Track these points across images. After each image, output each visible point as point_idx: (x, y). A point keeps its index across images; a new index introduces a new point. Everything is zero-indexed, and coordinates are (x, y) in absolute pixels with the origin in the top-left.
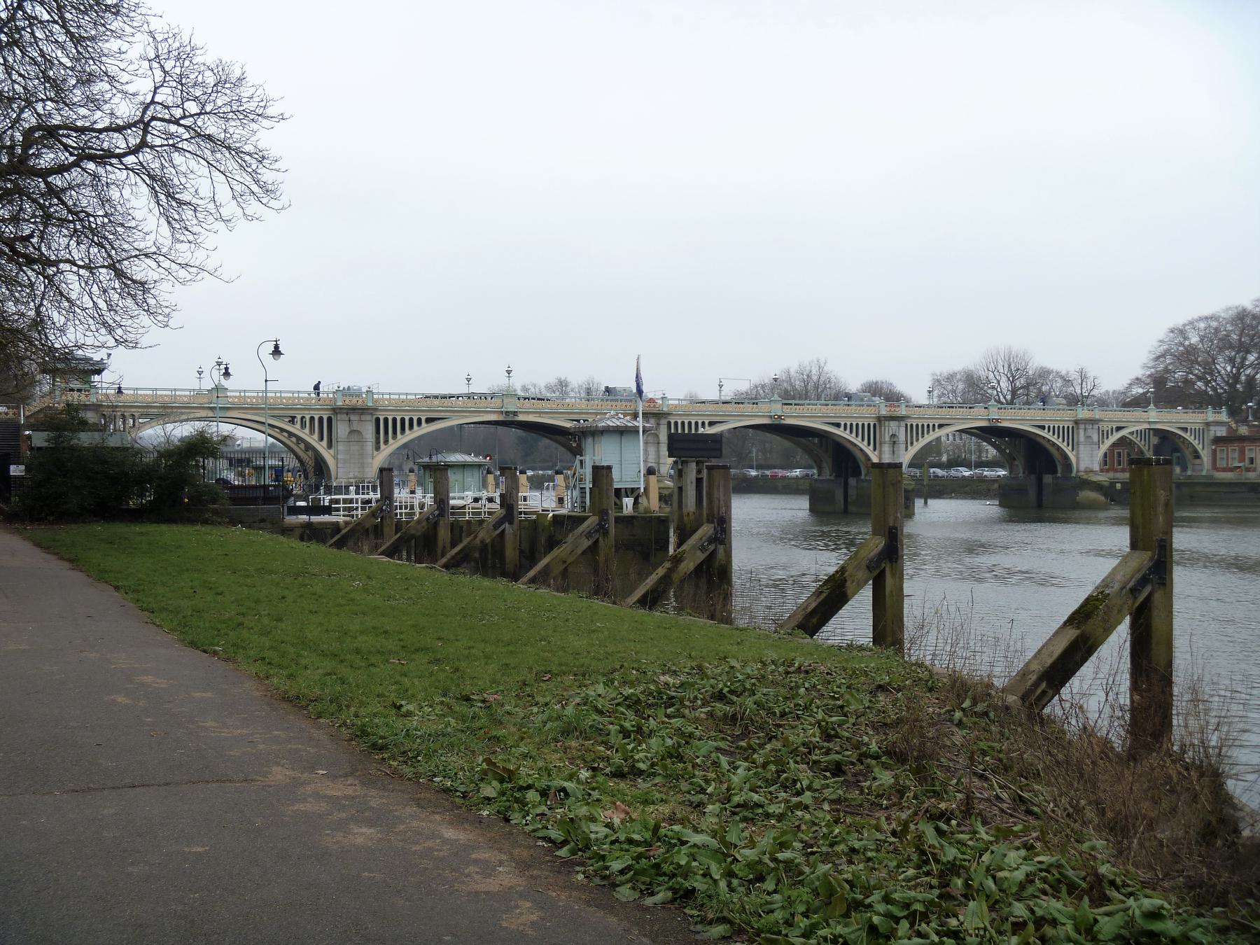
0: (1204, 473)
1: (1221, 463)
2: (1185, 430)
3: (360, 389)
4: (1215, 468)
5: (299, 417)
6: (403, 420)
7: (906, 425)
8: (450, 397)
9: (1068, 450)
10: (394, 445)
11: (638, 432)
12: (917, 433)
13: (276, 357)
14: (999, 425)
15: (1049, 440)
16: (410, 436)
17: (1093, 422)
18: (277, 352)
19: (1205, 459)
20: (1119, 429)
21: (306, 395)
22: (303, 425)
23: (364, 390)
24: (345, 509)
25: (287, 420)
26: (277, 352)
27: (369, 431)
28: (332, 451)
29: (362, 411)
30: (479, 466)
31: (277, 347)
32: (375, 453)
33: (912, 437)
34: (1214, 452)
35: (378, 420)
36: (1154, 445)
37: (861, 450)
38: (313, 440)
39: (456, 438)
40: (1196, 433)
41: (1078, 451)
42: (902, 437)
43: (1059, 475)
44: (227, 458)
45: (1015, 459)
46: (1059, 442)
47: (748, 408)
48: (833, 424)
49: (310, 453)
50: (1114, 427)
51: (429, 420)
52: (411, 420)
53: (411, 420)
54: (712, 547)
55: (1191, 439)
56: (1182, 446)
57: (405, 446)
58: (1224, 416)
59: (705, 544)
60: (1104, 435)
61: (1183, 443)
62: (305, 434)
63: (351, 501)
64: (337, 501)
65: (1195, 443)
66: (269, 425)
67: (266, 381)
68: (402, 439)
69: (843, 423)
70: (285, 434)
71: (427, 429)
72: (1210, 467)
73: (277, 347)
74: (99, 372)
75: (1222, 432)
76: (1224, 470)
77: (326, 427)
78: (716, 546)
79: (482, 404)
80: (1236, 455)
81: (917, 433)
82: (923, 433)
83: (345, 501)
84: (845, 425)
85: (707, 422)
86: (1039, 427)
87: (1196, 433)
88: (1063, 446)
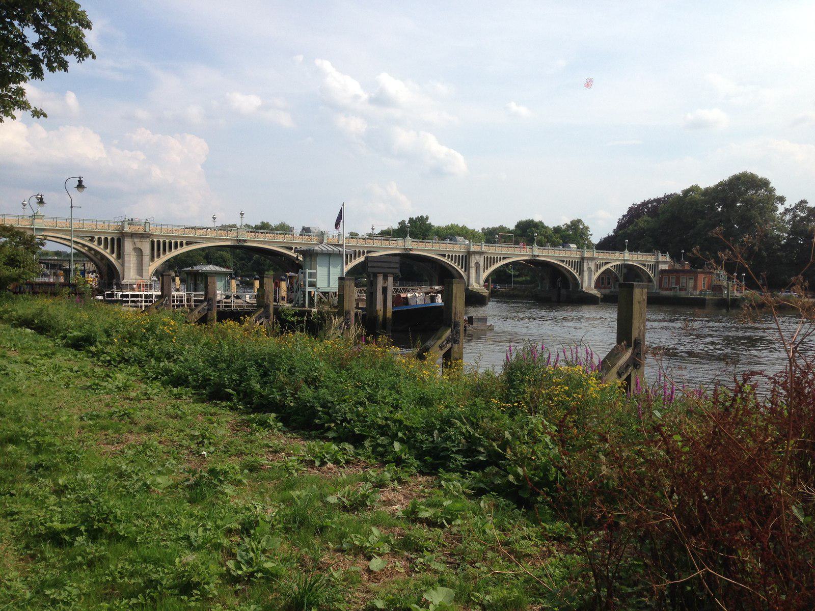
0: (654, 291)
1: (665, 285)
2: (644, 265)
3: (140, 220)
4: (660, 287)
5: (96, 237)
6: (164, 243)
7: (153, 242)
8: (202, 229)
9: (577, 275)
10: (164, 258)
11: (342, 255)
12: (490, 262)
13: (80, 189)
14: (411, 252)
15: (566, 268)
16: (175, 253)
17: (592, 259)
18: (80, 185)
19: (655, 282)
20: (606, 263)
21: (102, 223)
22: (100, 243)
23: (144, 221)
24: (132, 301)
25: (88, 239)
26: (80, 185)
27: (146, 247)
28: (120, 261)
29: (143, 236)
30: (225, 274)
31: (80, 182)
32: (151, 263)
33: (487, 264)
34: (661, 279)
35: (153, 242)
36: (624, 274)
37: (457, 271)
38: (107, 253)
39: (209, 255)
40: (650, 267)
41: (583, 276)
42: (593, 268)
43: (570, 289)
44: (45, 263)
45: (544, 279)
46: (572, 270)
47: (223, 235)
48: (561, 260)
49: (104, 262)
50: (365, 251)
51: (188, 244)
52: (170, 243)
53: (170, 243)
54: (449, 345)
55: (647, 271)
56: (642, 274)
57: (175, 258)
58: (667, 258)
59: (445, 343)
60: (598, 267)
61: (643, 273)
62: (100, 249)
63: (137, 296)
64: (127, 296)
65: (650, 273)
66: (74, 241)
67: (72, 207)
68: (170, 255)
69: (294, 247)
70: (86, 248)
71: (186, 249)
72: (658, 287)
73: (80, 182)
74: (65, 71)
75: (665, 267)
76: (667, 289)
77: (117, 243)
78: (452, 345)
79: (223, 235)
80: (674, 281)
81: (490, 262)
82: (494, 262)
83: (133, 296)
84: (449, 255)
85: (184, 242)
86: (642, 264)
87: (650, 267)
88: (574, 272)
